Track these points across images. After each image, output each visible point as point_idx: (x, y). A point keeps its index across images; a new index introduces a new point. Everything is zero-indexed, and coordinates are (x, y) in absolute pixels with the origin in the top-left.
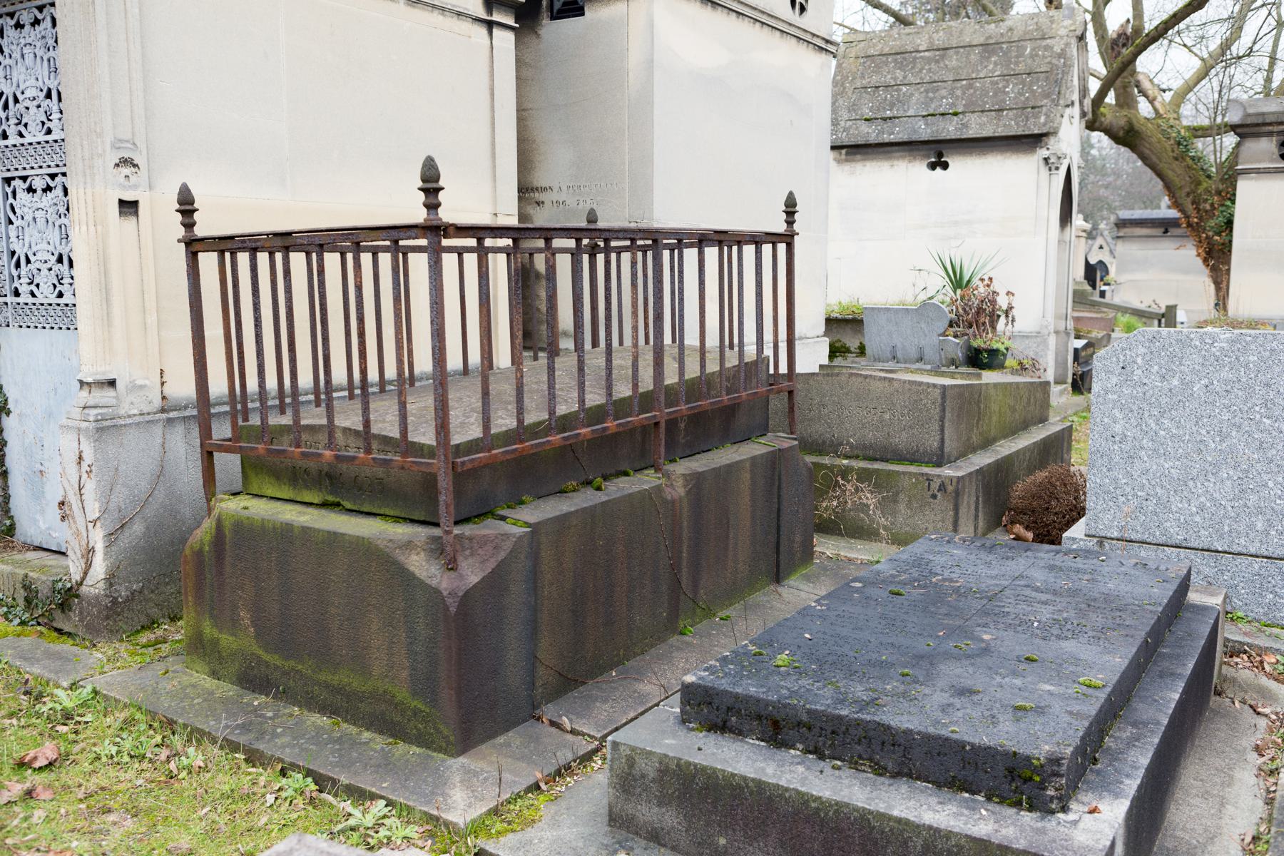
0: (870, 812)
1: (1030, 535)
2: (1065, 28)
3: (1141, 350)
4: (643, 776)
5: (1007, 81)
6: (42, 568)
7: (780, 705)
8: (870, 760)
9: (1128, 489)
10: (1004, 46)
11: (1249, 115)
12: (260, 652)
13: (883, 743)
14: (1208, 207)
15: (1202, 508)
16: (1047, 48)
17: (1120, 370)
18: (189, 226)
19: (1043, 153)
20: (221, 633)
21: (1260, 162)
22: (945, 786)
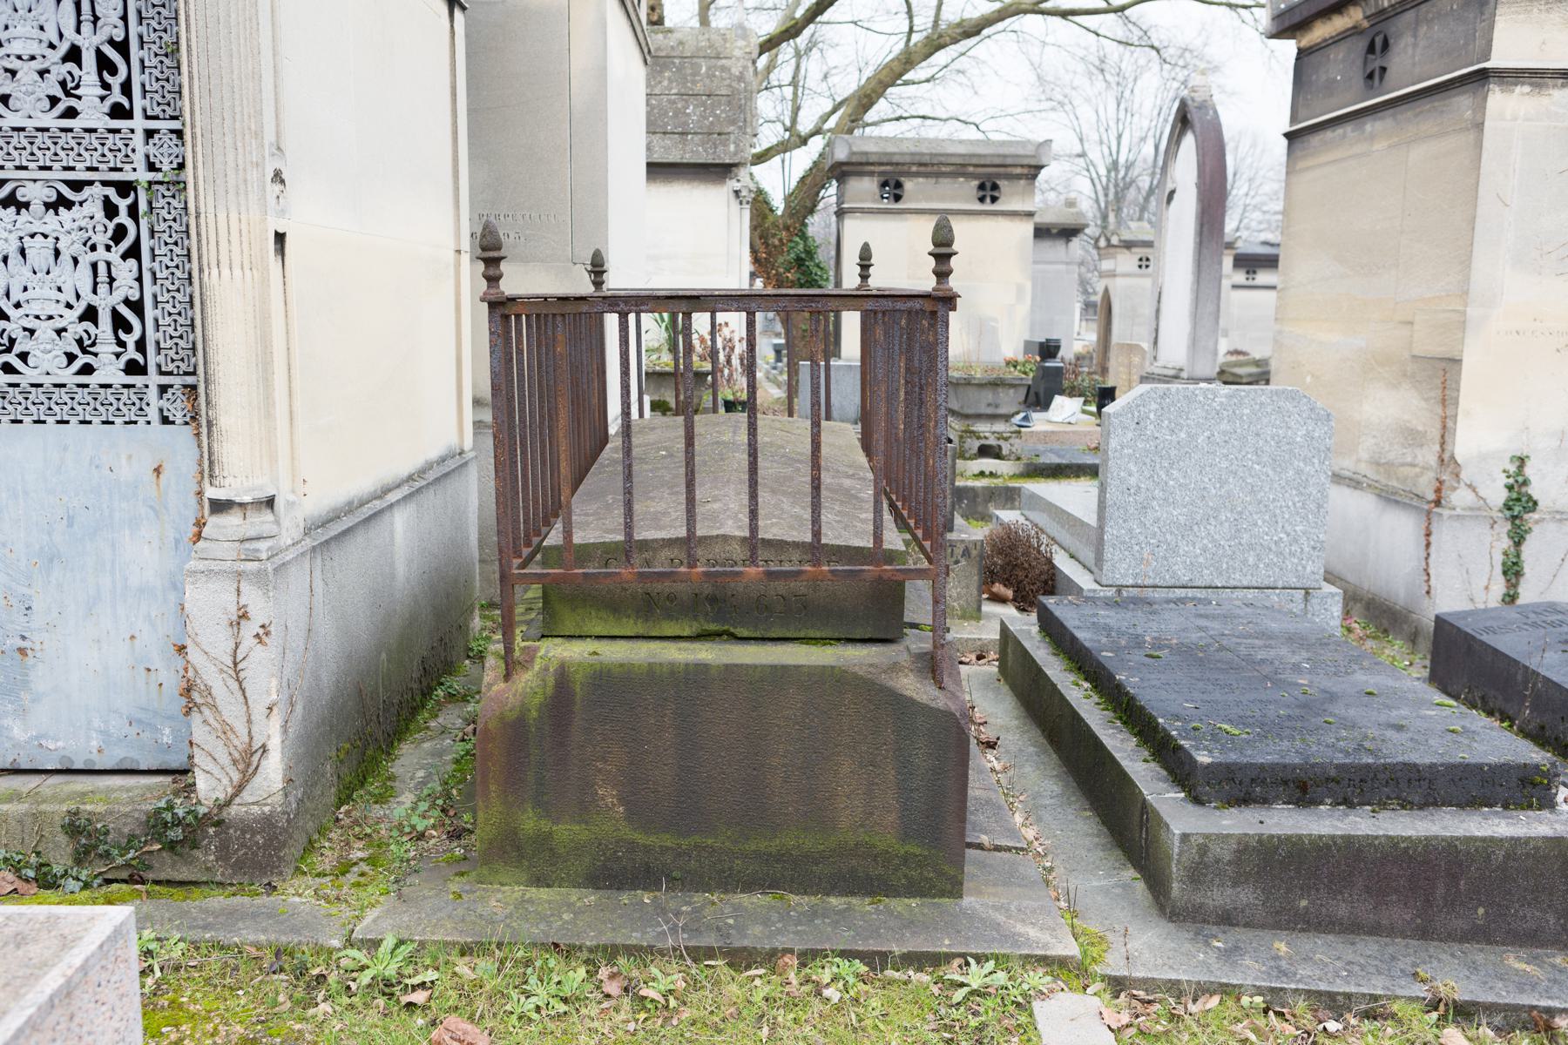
0: (1458, 839)
1: (1010, 593)
2: (740, 48)
3: (1154, 406)
4: (1217, 861)
5: (686, 101)
6: (55, 798)
7: (1307, 767)
8: (1398, 798)
9: (1142, 538)
10: (677, 61)
11: (854, 153)
12: (640, 838)
13: (1409, 781)
14: (777, 242)
15: (1204, 550)
16: (723, 69)
17: (1134, 425)
18: (493, 280)
19: (733, 184)
20: (556, 822)
21: (862, 201)
22: (1467, 805)
